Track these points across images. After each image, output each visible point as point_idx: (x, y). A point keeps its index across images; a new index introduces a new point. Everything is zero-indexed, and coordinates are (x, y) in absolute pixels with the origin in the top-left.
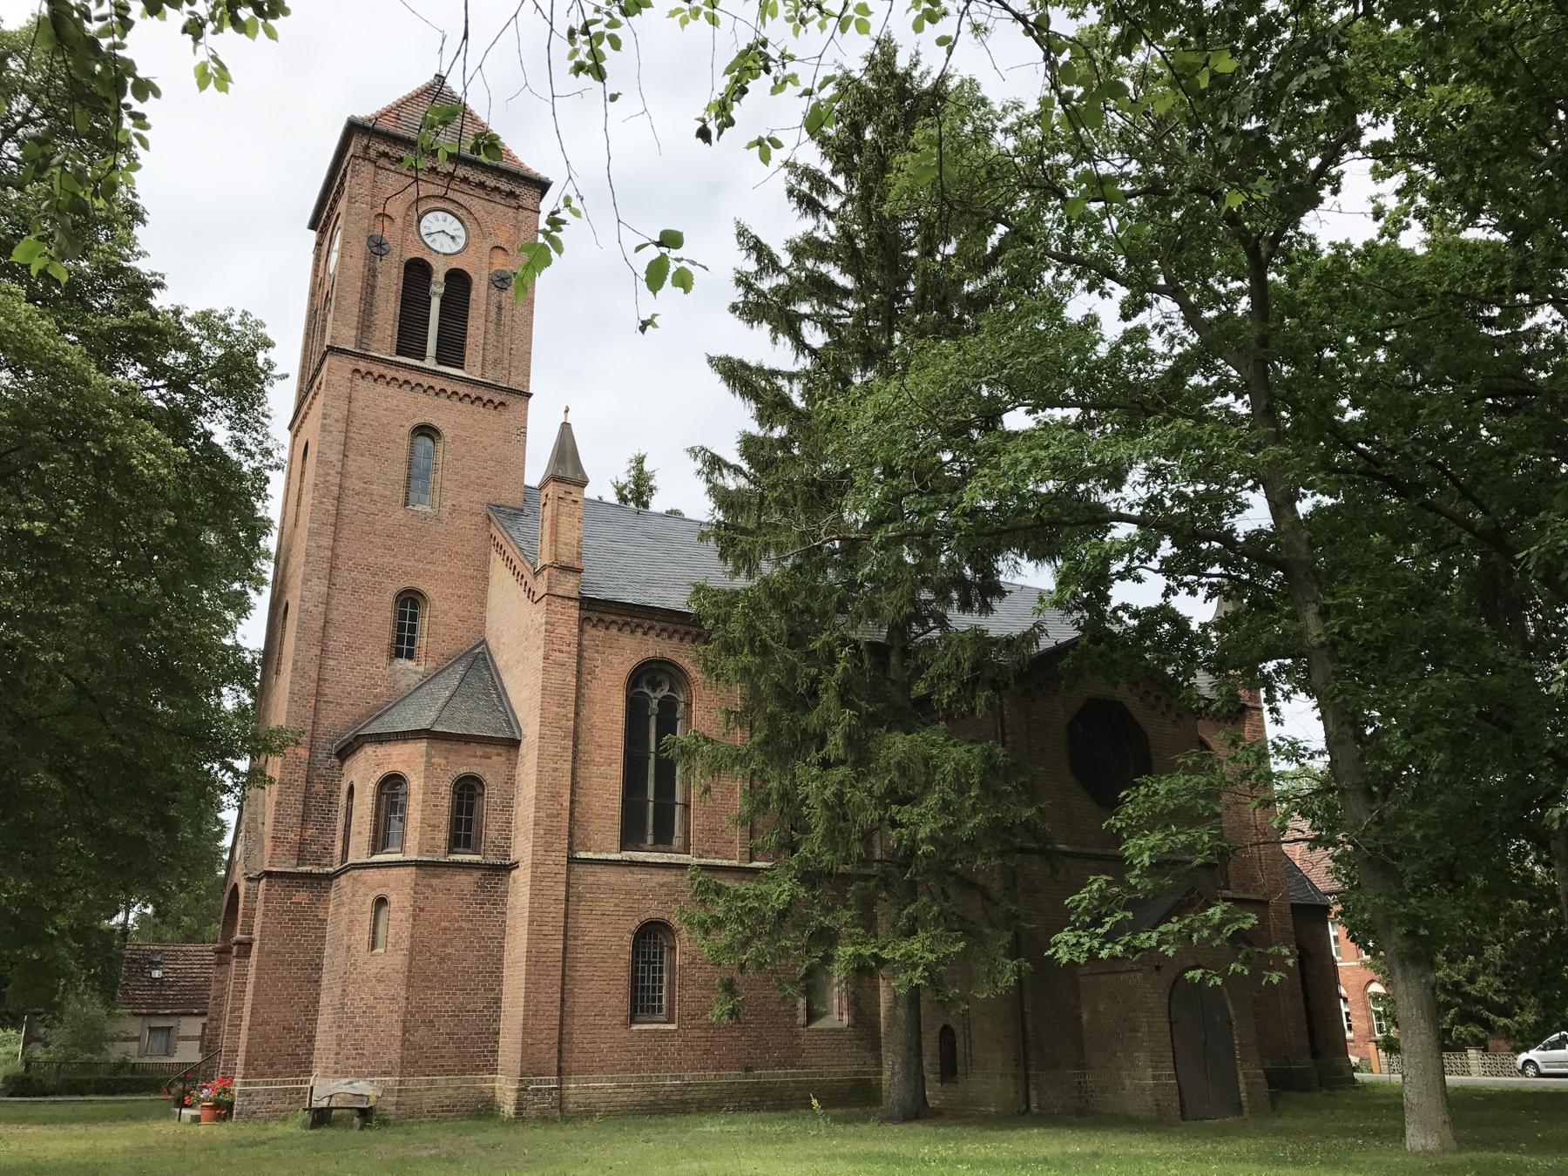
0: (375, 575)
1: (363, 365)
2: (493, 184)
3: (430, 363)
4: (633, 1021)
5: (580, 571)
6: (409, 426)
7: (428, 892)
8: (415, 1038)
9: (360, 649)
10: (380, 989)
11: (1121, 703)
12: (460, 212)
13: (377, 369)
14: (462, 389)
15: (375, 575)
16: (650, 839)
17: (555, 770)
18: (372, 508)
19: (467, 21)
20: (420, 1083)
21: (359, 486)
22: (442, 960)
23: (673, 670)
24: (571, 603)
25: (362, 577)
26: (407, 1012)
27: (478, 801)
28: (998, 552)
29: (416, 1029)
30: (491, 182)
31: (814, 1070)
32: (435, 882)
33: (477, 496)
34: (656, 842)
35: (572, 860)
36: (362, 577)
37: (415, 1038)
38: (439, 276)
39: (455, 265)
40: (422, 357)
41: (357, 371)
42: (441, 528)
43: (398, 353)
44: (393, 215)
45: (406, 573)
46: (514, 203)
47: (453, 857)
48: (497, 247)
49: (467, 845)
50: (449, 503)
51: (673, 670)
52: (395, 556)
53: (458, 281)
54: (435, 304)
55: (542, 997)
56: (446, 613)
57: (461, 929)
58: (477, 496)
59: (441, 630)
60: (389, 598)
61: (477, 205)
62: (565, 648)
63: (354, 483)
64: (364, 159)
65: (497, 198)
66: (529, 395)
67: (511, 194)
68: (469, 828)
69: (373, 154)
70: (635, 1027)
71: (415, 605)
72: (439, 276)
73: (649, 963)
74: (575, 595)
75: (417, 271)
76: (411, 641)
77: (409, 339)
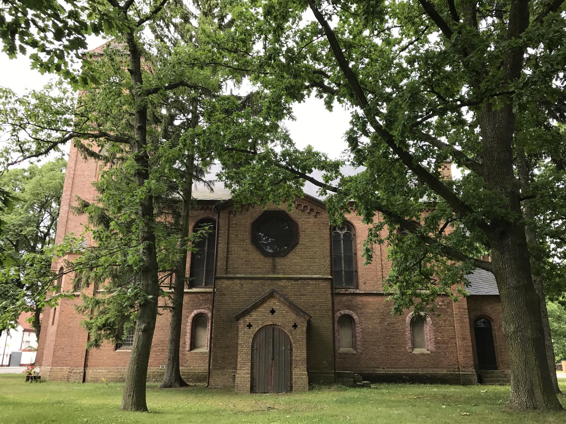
4: (116, 349)
7: (65, 305)
8: (58, 354)
11: (284, 211)
16: (204, 284)
20: (58, 369)
21: (80, 173)
22: (69, 328)
23: (349, 224)
26: (55, 345)
29: (58, 351)
31: (192, 368)
32: (68, 302)
34: (206, 285)
35: (333, 294)
37: (58, 354)
51: (349, 224)
55: (81, 340)
63: (78, 173)
70: (117, 351)
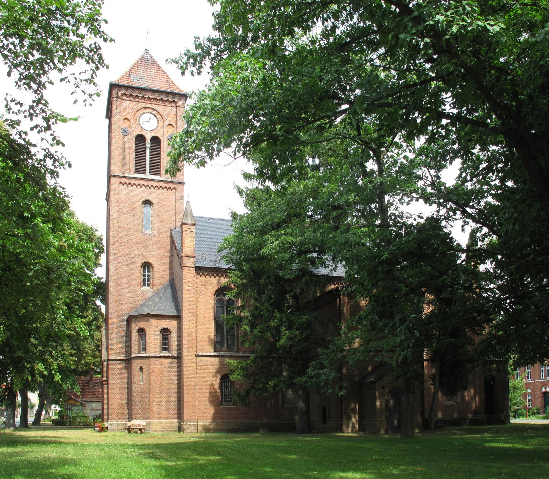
0: (133, 258)
1: (123, 180)
2: (165, 99)
3: (148, 176)
4: (221, 405)
5: (194, 257)
6: (141, 201)
9: (131, 284)
10: (143, 395)
12: (155, 113)
13: (128, 181)
14: (159, 184)
15: (133, 258)
17: (189, 327)
18: (131, 234)
19: (108, 198)
24: (192, 269)
25: (129, 259)
27: (169, 336)
28: (512, 179)
30: (132, 182)
32: (157, 362)
33: (167, 225)
36: (129, 259)
38: (148, 140)
39: (154, 135)
40: (144, 172)
41: (121, 183)
42: (155, 238)
43: (137, 171)
44: (130, 118)
45: (144, 256)
46: (174, 105)
47: (161, 354)
48: (170, 125)
49: (167, 350)
50: (157, 229)
52: (140, 250)
53: (156, 140)
54: (148, 151)
56: (159, 269)
57: (166, 377)
58: (167, 225)
59: (158, 276)
60: (139, 265)
61: (160, 108)
62: (191, 285)
64: (117, 98)
65: (168, 104)
66: (184, 184)
67: (174, 102)
68: (167, 345)
69: (120, 94)
70: (221, 406)
71: (148, 268)
72: (148, 140)
73: (226, 387)
74: (193, 266)
75: (140, 138)
76: (148, 280)
77: (140, 168)
